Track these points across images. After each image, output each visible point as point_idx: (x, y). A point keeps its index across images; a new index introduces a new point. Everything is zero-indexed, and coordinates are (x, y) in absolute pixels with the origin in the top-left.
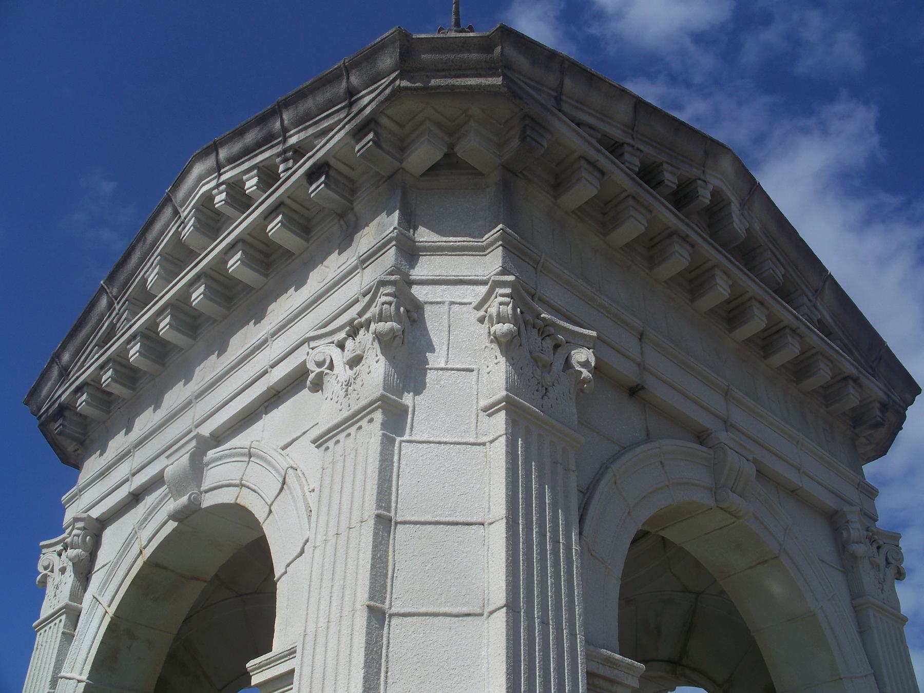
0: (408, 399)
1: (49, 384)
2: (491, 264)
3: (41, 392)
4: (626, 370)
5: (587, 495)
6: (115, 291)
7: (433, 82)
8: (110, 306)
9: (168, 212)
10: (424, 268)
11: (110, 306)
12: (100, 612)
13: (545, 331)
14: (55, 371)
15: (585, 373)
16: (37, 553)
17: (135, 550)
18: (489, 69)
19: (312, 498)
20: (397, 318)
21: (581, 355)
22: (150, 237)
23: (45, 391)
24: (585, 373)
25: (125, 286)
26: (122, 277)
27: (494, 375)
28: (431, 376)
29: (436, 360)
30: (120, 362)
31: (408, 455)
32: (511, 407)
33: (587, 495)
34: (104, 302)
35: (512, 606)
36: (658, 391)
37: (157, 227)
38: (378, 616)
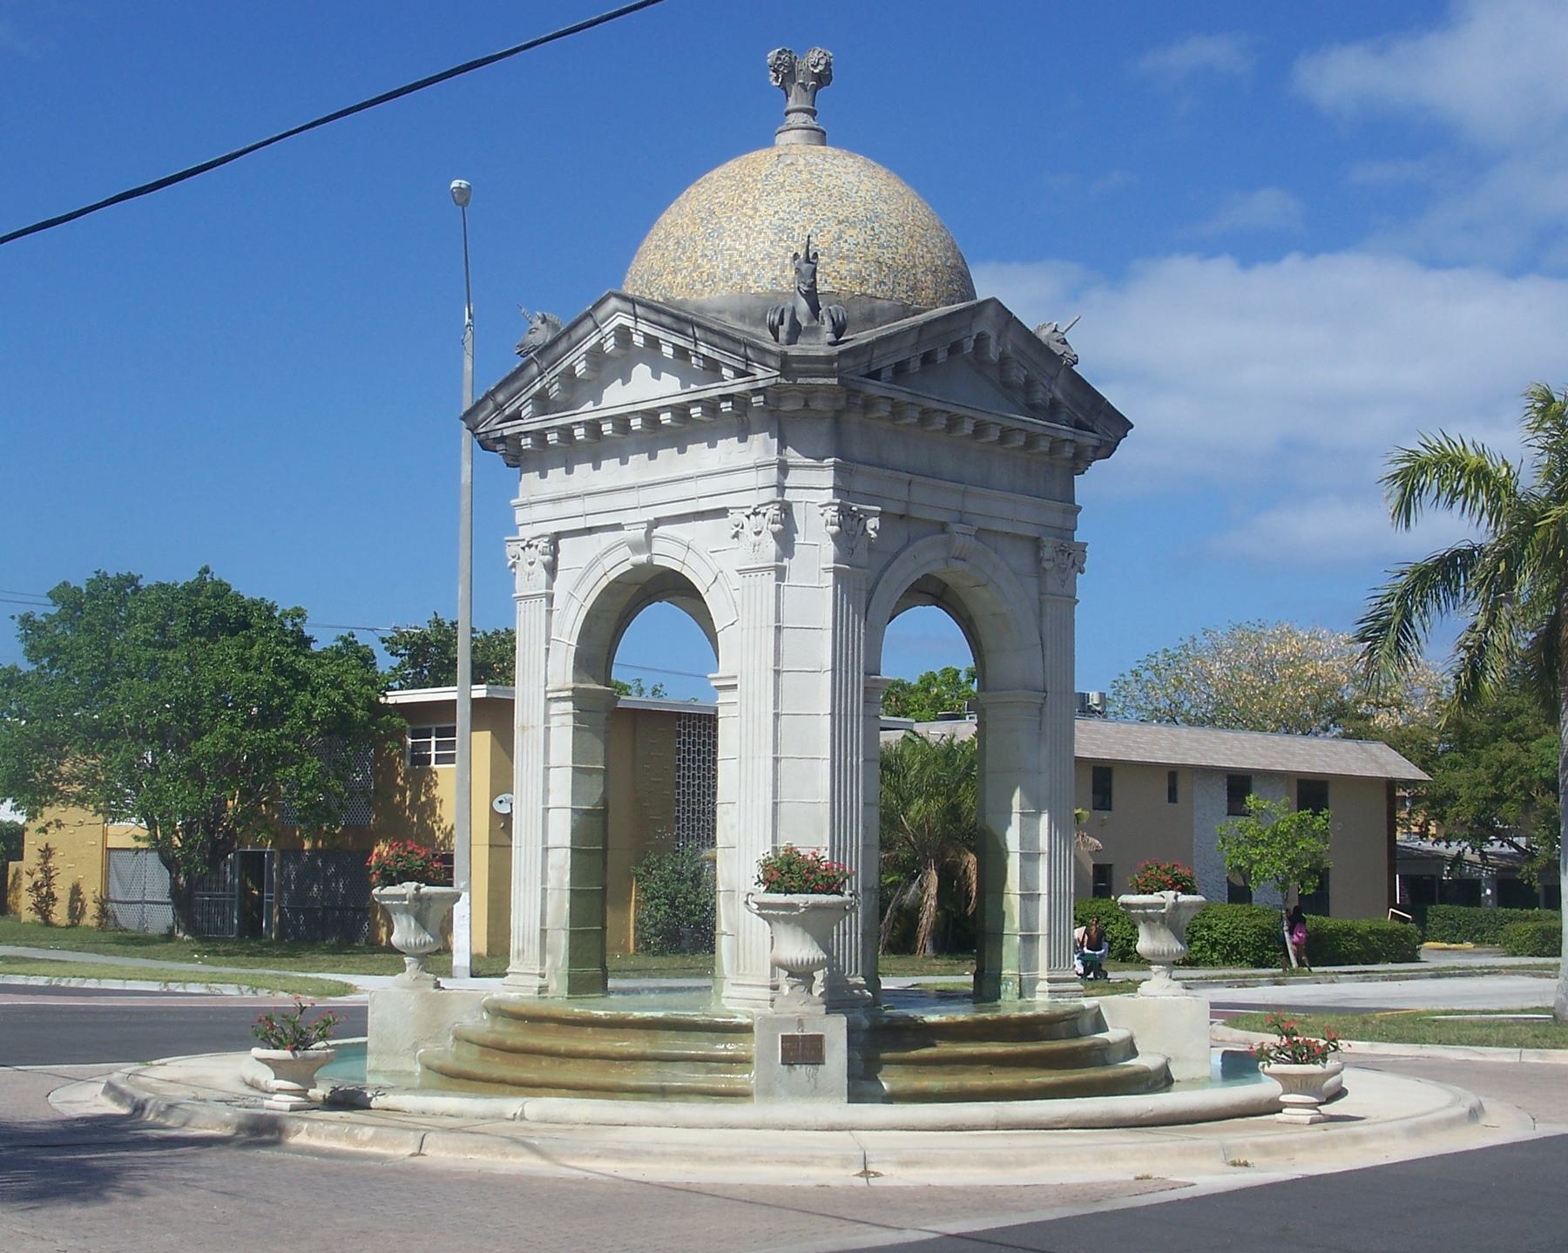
0: (786, 562)
2: (827, 478)
4: (896, 509)
5: (871, 593)
7: (800, 381)
8: (541, 373)
9: (589, 324)
10: (793, 478)
11: (541, 373)
12: (575, 605)
13: (853, 515)
14: (491, 405)
15: (874, 534)
16: (502, 545)
17: (599, 571)
18: (830, 374)
19: (737, 595)
20: (782, 522)
21: (873, 523)
23: (481, 417)
24: (874, 534)
25: (554, 362)
26: (550, 356)
27: (829, 550)
28: (796, 548)
29: (799, 538)
30: (566, 432)
31: (787, 592)
32: (837, 572)
33: (871, 593)
34: (534, 369)
35: (832, 714)
36: (917, 513)
38: (777, 673)
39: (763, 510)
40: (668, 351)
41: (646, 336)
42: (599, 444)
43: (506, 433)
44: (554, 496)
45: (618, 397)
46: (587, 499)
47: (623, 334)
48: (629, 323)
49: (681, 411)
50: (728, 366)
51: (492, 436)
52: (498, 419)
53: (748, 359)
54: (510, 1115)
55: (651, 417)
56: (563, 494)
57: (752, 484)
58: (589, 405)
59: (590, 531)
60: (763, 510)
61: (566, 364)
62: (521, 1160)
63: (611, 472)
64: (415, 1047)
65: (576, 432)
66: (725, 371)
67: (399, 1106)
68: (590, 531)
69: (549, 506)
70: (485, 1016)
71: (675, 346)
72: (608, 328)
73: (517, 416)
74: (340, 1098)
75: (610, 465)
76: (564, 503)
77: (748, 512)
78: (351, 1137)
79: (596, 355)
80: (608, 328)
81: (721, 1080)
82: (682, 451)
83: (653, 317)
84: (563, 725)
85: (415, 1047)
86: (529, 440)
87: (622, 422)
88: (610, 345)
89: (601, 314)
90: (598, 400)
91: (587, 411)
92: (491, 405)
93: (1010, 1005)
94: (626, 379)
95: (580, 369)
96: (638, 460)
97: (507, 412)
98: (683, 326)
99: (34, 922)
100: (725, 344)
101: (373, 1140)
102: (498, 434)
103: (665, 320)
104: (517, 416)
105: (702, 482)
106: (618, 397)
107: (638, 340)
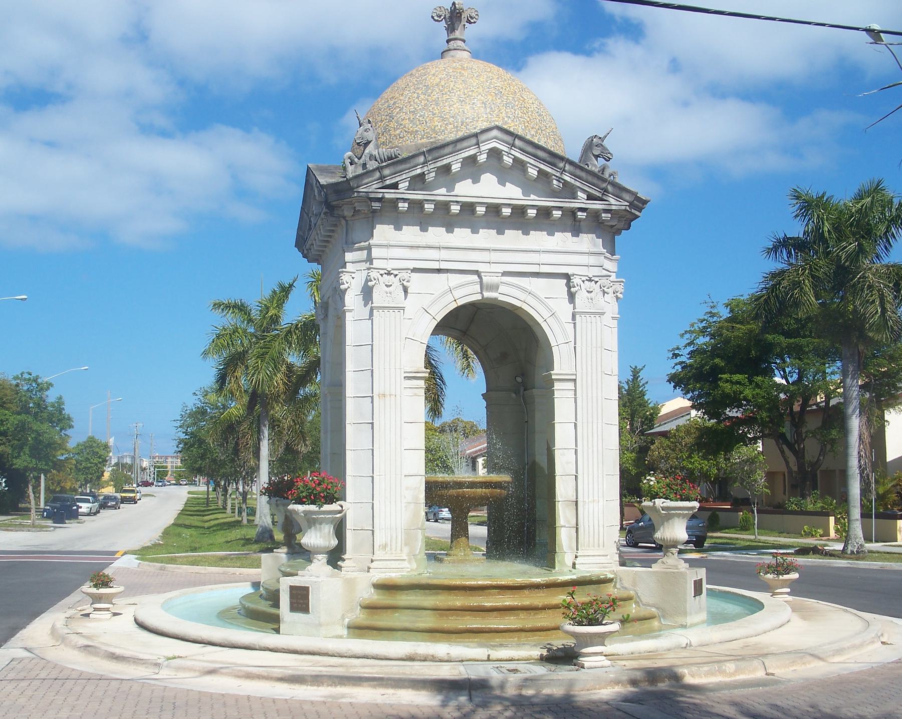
1: (370, 179)
3: (363, 180)
6: (430, 158)
9: (474, 141)
14: (377, 175)
22: (459, 146)
23: (366, 181)
25: (436, 159)
26: (435, 154)
34: (421, 159)
37: (465, 144)
39: (596, 279)
40: (533, 172)
41: (516, 159)
42: (445, 216)
43: (387, 196)
44: (410, 244)
45: (465, 190)
46: (492, 253)
48: (503, 147)
50: (584, 191)
51: (372, 195)
52: (380, 185)
53: (606, 190)
54: (684, 645)
55: (494, 209)
57: (586, 263)
58: (443, 191)
59: (439, 271)
61: (445, 162)
62: (812, 665)
63: (462, 236)
64: (343, 618)
66: (579, 194)
67: (615, 652)
68: (439, 271)
69: (408, 250)
70: (372, 590)
71: (540, 172)
72: (485, 147)
73: (395, 186)
76: (421, 250)
77: (584, 278)
78: (722, 672)
80: (485, 147)
83: (530, 149)
84: (416, 395)
85: (343, 618)
86: (406, 205)
88: (482, 158)
89: (482, 137)
90: (451, 188)
91: (441, 194)
92: (377, 175)
93: (563, 572)
94: (476, 180)
95: (456, 167)
97: (388, 182)
98: (556, 161)
101: (736, 672)
102: (380, 196)
104: (395, 186)
105: (543, 255)
106: (465, 190)
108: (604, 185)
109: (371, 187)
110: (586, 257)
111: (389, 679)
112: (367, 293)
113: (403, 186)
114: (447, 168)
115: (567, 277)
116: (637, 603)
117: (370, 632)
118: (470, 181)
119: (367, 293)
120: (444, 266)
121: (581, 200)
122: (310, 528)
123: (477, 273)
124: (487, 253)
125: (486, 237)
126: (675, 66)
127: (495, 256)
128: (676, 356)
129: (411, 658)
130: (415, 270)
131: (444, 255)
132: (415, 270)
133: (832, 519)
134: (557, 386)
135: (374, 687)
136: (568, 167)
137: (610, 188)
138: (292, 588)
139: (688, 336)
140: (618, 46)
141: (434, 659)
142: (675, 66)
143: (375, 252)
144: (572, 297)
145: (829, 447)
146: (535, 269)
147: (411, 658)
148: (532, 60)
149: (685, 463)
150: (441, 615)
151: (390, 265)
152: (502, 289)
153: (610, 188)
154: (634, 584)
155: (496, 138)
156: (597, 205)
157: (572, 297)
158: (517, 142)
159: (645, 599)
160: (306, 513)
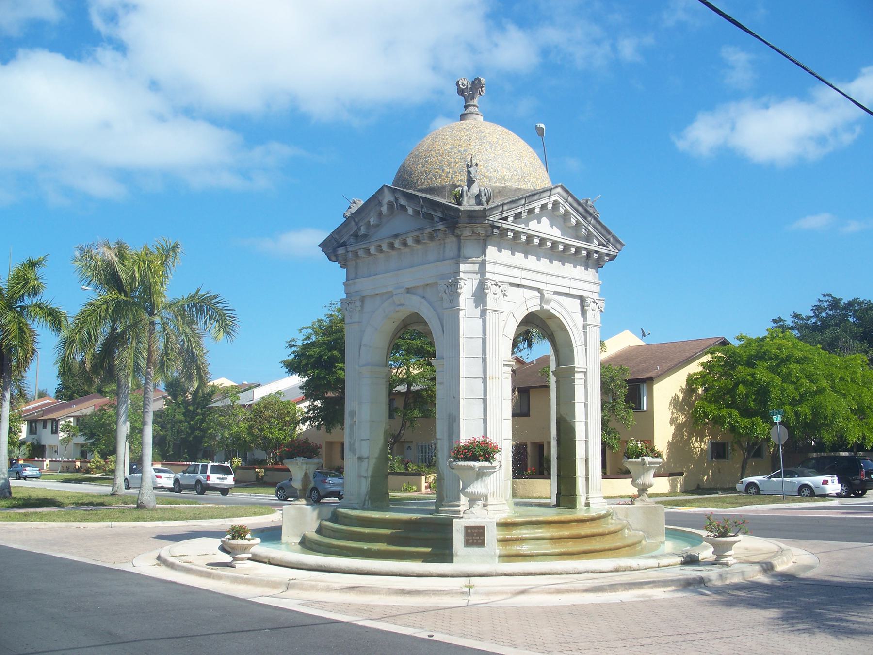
9: (548, 193)
47: (556, 204)
49: (555, 244)
51: (496, 224)
53: (609, 241)
55: (543, 241)
56: (514, 265)
58: (523, 226)
59: (519, 286)
60: (500, 284)
63: (531, 262)
65: (509, 234)
68: (519, 286)
72: (553, 199)
73: (506, 219)
74: (689, 559)
75: (532, 258)
79: (543, 207)
81: (596, 544)
82: (575, 267)
83: (575, 205)
87: (530, 238)
88: (550, 206)
93: (581, 512)
96: (544, 261)
98: (587, 216)
99: (460, 443)
100: (603, 231)
102: (500, 225)
103: (581, 209)
104: (506, 219)
105: (573, 281)
107: (562, 211)
108: (609, 237)
109: (494, 217)
110: (591, 285)
111: (659, 581)
112: (480, 296)
113: (511, 219)
114: (531, 211)
115: (582, 299)
116: (628, 529)
117: (517, 558)
118: (536, 221)
119: (480, 296)
120: (524, 282)
121: (594, 246)
122: (477, 479)
123: (538, 290)
124: (545, 276)
125: (543, 264)
126: (154, 85)
127: (550, 279)
128: (291, 346)
129: (617, 570)
130: (512, 284)
131: (525, 274)
132: (512, 284)
133: (423, 478)
134: (576, 374)
135: (652, 588)
136: (593, 221)
137: (611, 239)
138: (467, 528)
139: (304, 331)
140: (106, 55)
141: (631, 569)
142: (154, 85)
143: (489, 267)
144: (584, 312)
145: (408, 424)
146: (566, 291)
147: (617, 570)
148: (21, 52)
149: (265, 433)
150: (555, 543)
151: (498, 278)
152: (553, 304)
153: (611, 239)
154: (626, 516)
155: (558, 193)
156: (603, 250)
157: (584, 312)
158: (570, 199)
159: (634, 526)
160: (481, 468)
